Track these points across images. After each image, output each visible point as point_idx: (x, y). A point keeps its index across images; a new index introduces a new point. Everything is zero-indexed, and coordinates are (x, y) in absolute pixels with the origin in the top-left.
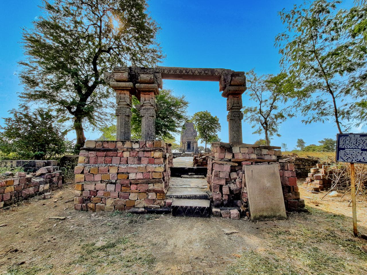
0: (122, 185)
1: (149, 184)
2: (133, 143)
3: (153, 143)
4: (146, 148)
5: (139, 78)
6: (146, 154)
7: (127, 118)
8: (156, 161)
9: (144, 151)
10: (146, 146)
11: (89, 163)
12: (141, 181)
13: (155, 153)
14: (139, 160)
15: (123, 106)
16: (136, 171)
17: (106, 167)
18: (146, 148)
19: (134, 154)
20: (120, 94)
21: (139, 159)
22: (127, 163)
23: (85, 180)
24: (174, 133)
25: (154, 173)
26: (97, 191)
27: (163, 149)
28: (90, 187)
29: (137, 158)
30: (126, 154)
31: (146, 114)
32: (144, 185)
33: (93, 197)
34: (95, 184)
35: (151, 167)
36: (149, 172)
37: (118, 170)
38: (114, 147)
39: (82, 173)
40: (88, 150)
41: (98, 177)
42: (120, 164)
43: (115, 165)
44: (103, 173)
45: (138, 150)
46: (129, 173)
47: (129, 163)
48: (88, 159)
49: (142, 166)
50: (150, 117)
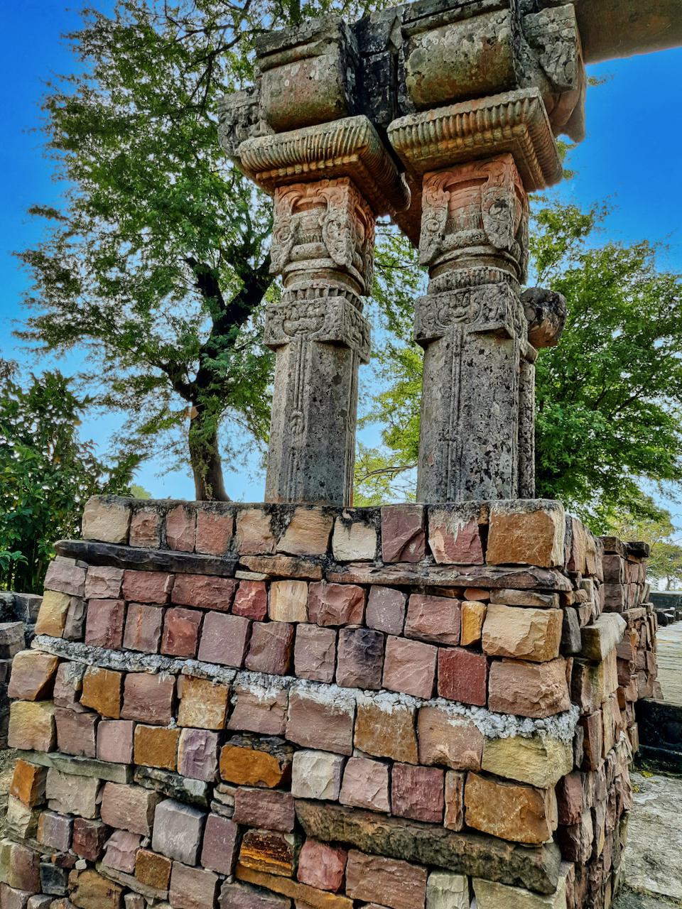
0: (243, 828)
1: (432, 868)
2: (338, 524)
3: (484, 529)
4: (426, 562)
5: (407, 65)
6: (436, 617)
7: (329, 356)
8: (505, 681)
9: (407, 588)
10: (428, 551)
11: (82, 640)
12: (369, 829)
13: (498, 611)
14: (368, 656)
15: (309, 283)
16: (342, 737)
17: (164, 676)
18: (426, 562)
19: (340, 604)
20: (296, 209)
21: (374, 649)
22: (290, 671)
23: (54, 748)
24: (667, 484)
25: (476, 787)
26: (108, 831)
27: (563, 582)
28: (73, 795)
29: (356, 640)
30: (287, 601)
31: (456, 325)
32: (393, 867)
33: (81, 864)
34: (102, 783)
35: (457, 730)
36: (441, 765)
37: (230, 708)
38: (221, 547)
39: (45, 695)
40: (91, 556)
41: (116, 741)
42: (243, 667)
43: (212, 670)
44: (144, 715)
45: (364, 575)
46: (296, 747)
47: (299, 668)
48: (79, 616)
49: (385, 703)
50: (479, 343)
